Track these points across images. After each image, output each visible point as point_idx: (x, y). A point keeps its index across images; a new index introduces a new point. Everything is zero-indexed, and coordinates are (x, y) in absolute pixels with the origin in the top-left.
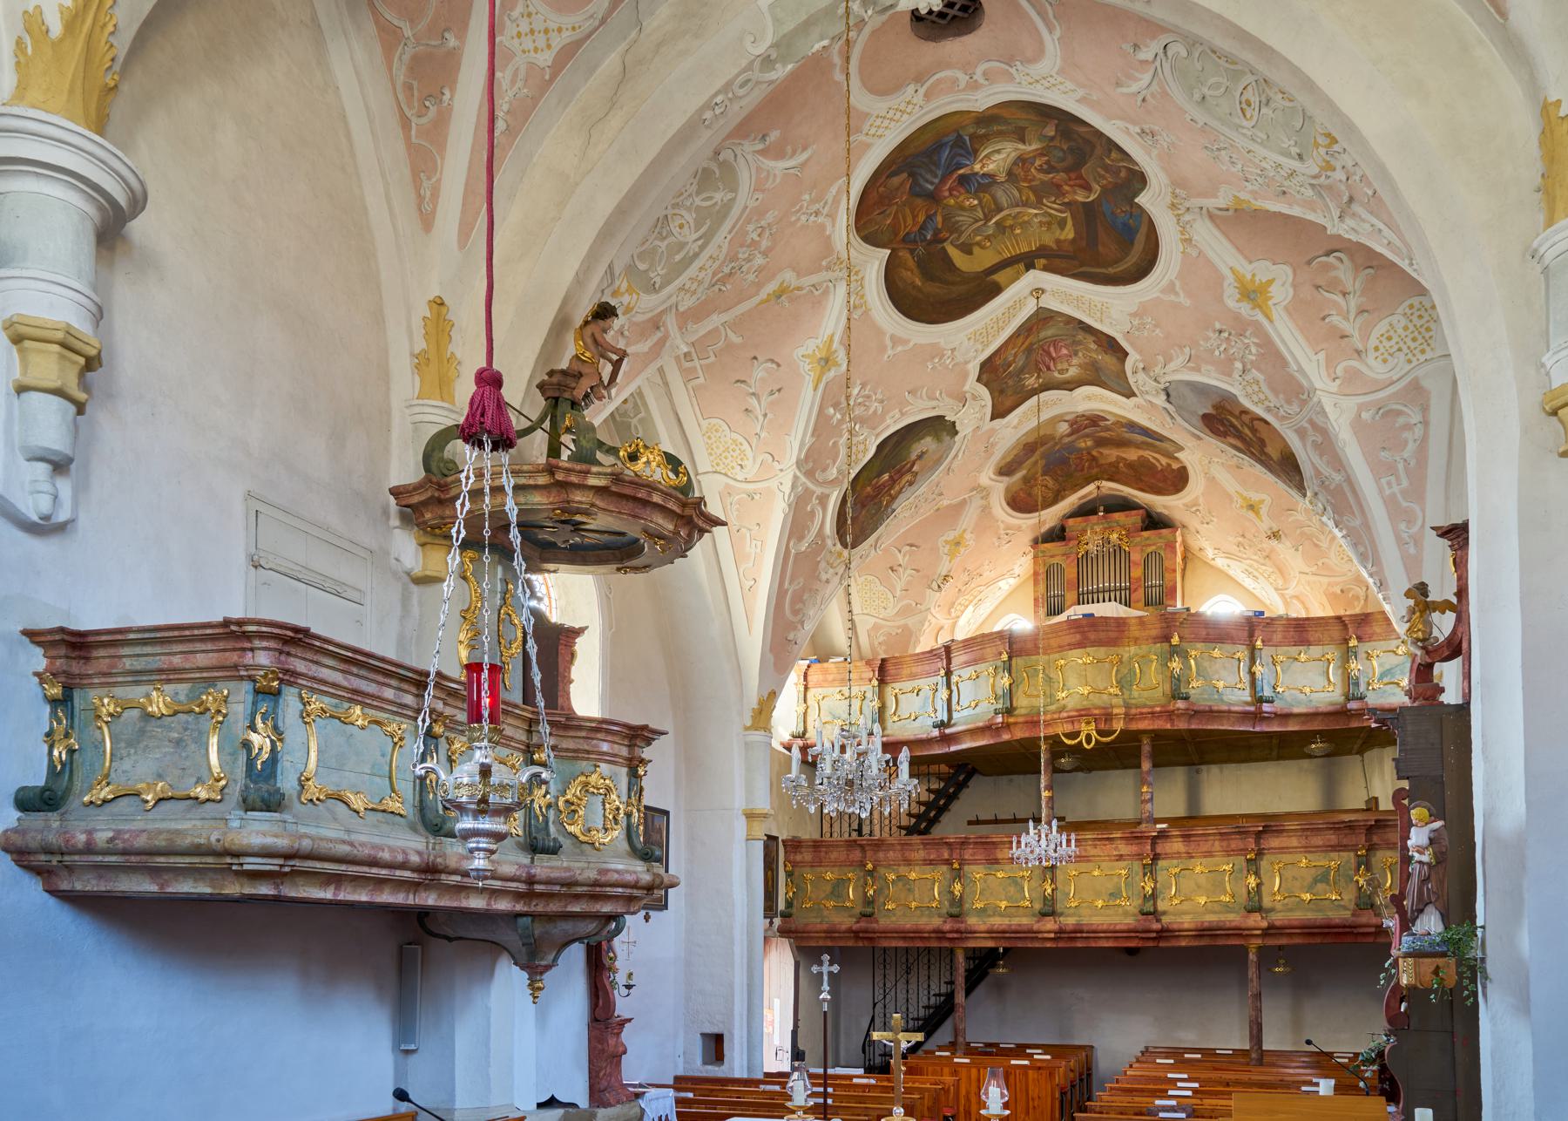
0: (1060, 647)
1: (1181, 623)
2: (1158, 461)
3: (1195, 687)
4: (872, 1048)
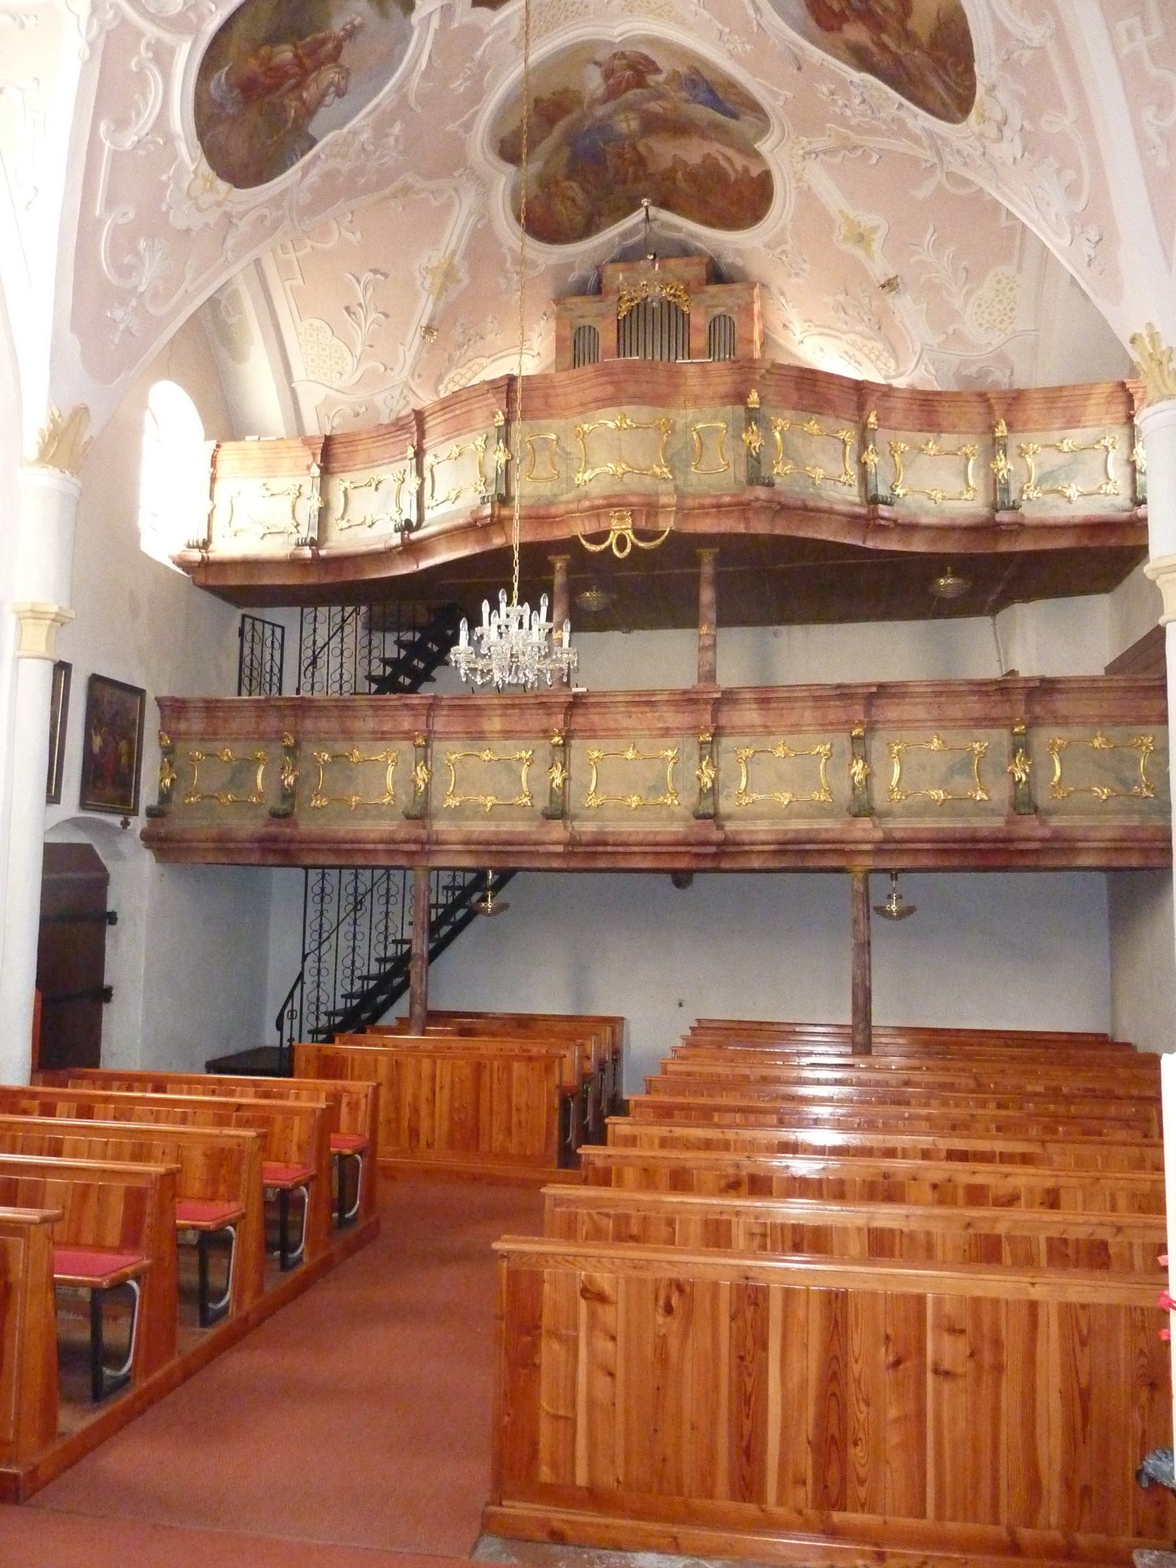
0: (582, 404)
1: (762, 377)
2: (729, 160)
3: (781, 471)
4: (296, 1022)
